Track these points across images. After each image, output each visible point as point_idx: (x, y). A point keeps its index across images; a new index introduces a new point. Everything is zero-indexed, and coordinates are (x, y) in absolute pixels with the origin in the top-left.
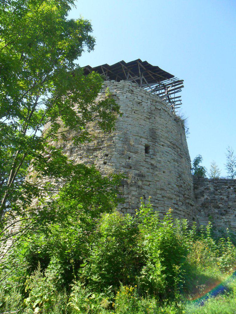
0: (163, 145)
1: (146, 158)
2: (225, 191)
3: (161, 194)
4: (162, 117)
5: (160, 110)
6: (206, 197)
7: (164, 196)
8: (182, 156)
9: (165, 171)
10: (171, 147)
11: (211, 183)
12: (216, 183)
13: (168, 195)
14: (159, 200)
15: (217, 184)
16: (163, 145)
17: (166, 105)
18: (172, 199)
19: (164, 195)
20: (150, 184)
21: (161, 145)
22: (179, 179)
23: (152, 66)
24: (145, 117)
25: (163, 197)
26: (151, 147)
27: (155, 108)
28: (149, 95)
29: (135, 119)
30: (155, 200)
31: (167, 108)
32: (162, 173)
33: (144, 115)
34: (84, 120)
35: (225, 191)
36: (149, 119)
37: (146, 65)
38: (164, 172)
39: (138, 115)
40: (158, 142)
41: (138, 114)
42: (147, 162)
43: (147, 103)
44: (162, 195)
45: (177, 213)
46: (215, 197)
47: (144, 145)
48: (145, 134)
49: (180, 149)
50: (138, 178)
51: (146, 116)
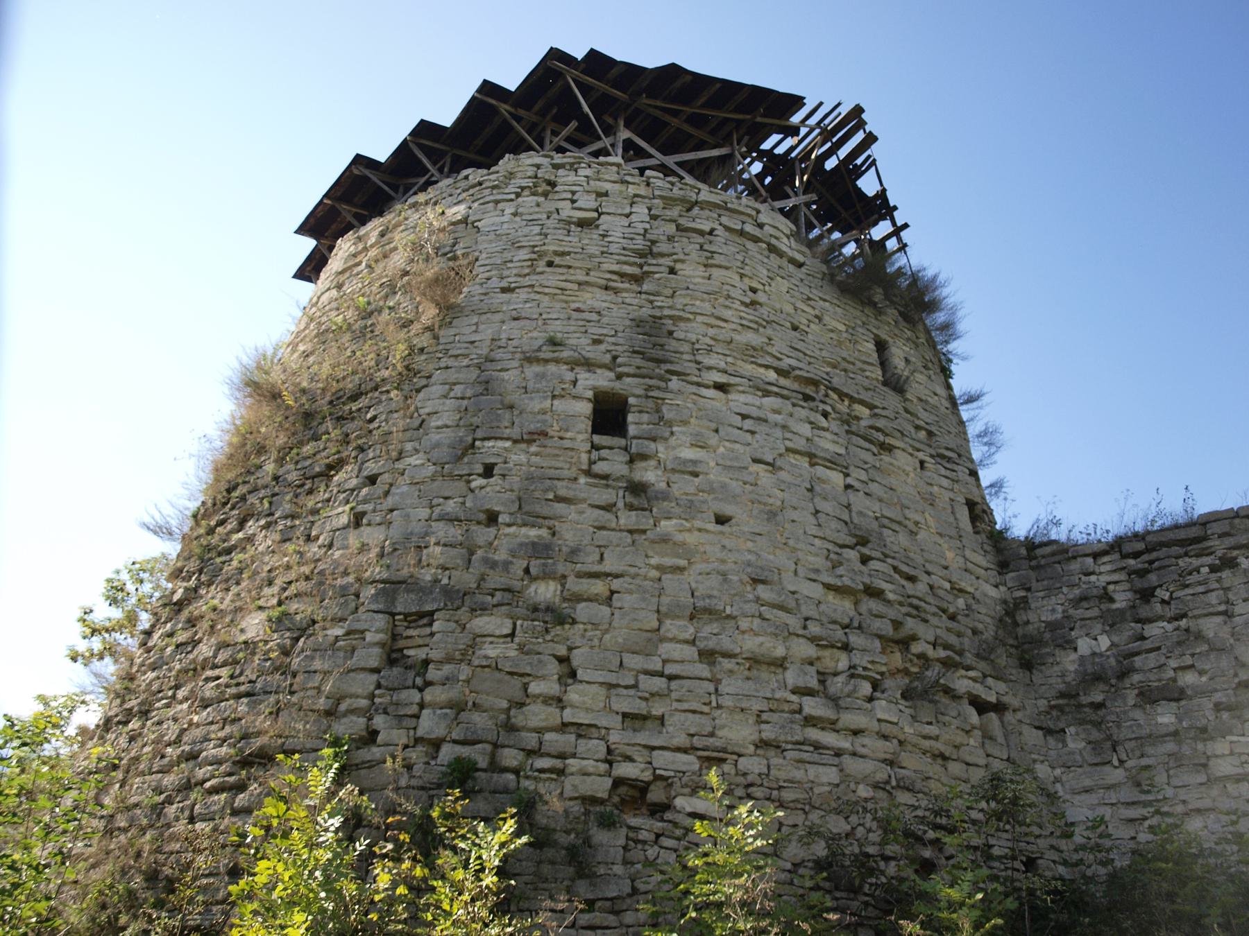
0: (721, 387)
1: (595, 455)
2: (1201, 589)
3: (693, 642)
4: (718, 260)
5: (711, 232)
6: (1084, 646)
7: (718, 648)
8: (889, 440)
9: (728, 510)
10: (785, 392)
11: (1106, 559)
12: (1136, 555)
13: (750, 644)
14: (671, 678)
15: (1146, 557)
16: (721, 387)
17: (754, 213)
18: (780, 664)
19: (712, 644)
20: (614, 587)
21: (707, 387)
22: (852, 555)
23: (642, 70)
24: (608, 276)
25: (708, 656)
26: (631, 400)
27: (678, 230)
28: (648, 184)
29: (547, 290)
30: (642, 677)
31: (766, 228)
32: (712, 526)
33: (605, 267)
34: (1090, 924)
35: (1201, 589)
36: (637, 279)
37: (678, 84)
38: (721, 520)
39: (565, 270)
40: (685, 374)
41: (570, 267)
42: (606, 477)
43: (628, 216)
44: (702, 645)
45: (817, 746)
46: (1146, 634)
47: (590, 394)
48: (603, 347)
49: (871, 407)
50: (534, 562)
51: (615, 268)
